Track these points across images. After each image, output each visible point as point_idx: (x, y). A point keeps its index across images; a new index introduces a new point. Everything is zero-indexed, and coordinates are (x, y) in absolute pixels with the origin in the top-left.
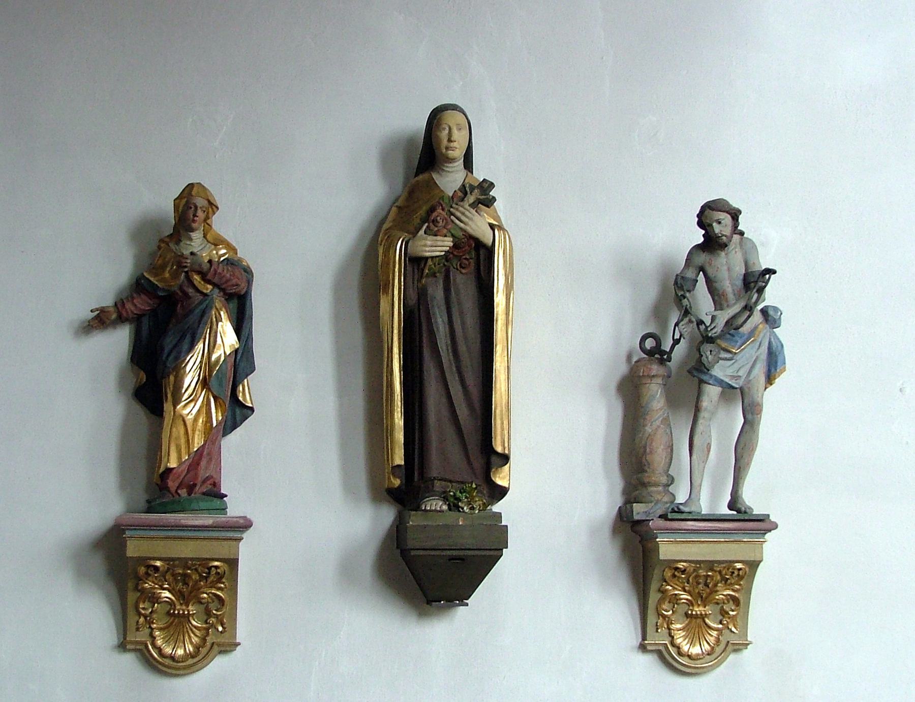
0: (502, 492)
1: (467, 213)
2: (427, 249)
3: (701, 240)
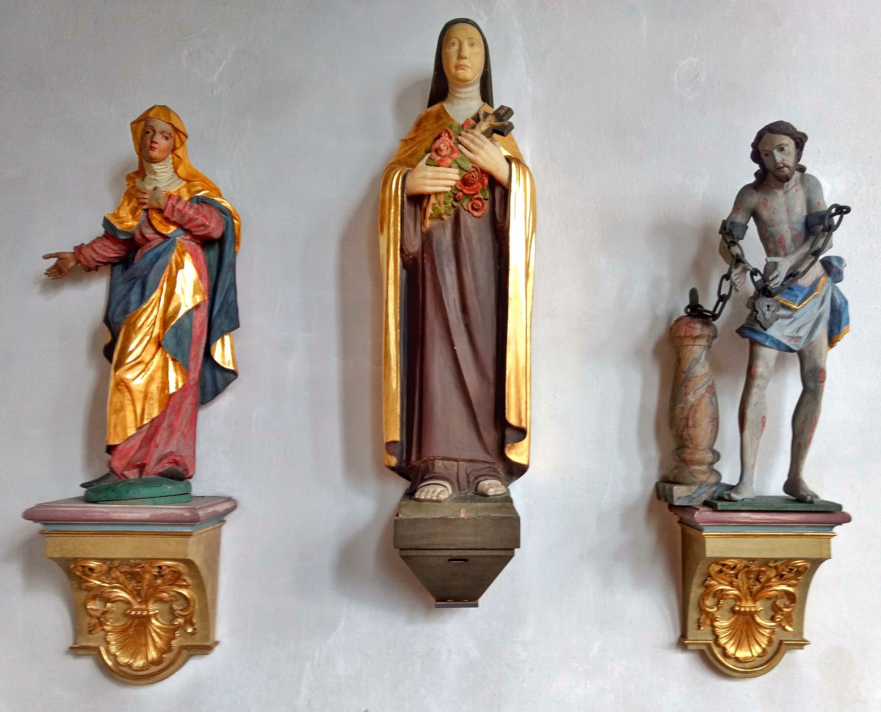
0: (517, 471)
1: (477, 140)
2: (429, 182)
3: (752, 179)
